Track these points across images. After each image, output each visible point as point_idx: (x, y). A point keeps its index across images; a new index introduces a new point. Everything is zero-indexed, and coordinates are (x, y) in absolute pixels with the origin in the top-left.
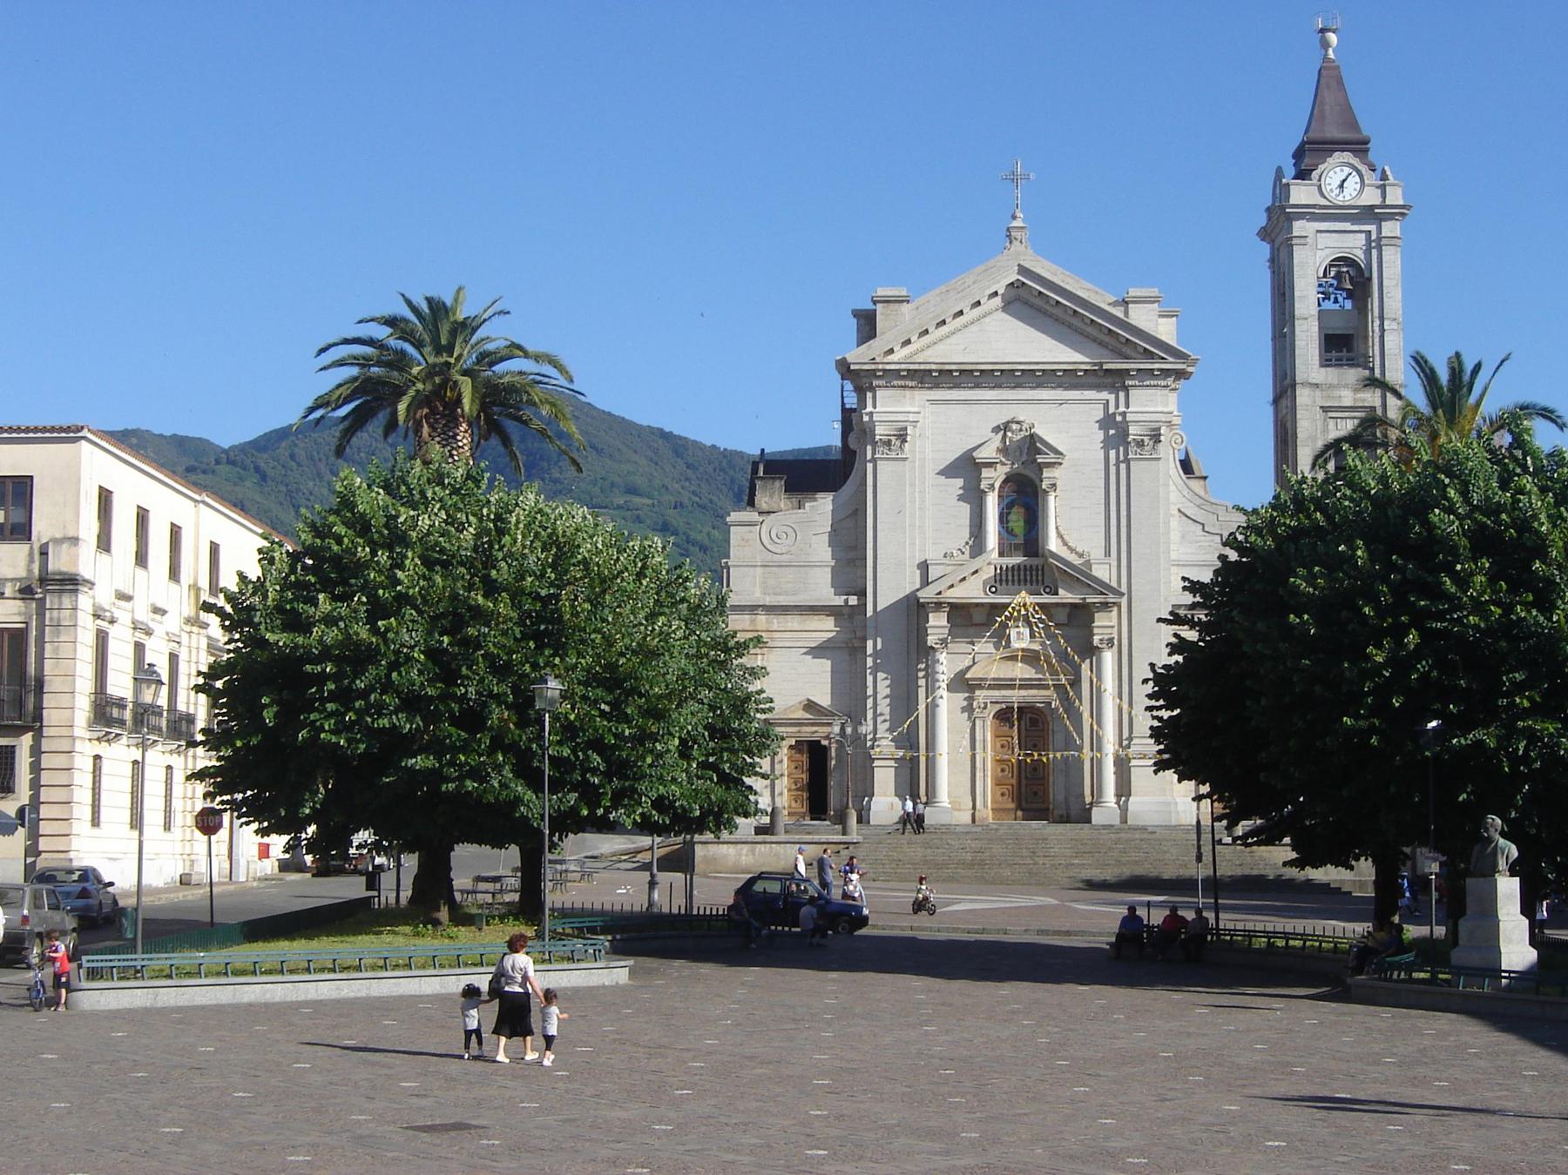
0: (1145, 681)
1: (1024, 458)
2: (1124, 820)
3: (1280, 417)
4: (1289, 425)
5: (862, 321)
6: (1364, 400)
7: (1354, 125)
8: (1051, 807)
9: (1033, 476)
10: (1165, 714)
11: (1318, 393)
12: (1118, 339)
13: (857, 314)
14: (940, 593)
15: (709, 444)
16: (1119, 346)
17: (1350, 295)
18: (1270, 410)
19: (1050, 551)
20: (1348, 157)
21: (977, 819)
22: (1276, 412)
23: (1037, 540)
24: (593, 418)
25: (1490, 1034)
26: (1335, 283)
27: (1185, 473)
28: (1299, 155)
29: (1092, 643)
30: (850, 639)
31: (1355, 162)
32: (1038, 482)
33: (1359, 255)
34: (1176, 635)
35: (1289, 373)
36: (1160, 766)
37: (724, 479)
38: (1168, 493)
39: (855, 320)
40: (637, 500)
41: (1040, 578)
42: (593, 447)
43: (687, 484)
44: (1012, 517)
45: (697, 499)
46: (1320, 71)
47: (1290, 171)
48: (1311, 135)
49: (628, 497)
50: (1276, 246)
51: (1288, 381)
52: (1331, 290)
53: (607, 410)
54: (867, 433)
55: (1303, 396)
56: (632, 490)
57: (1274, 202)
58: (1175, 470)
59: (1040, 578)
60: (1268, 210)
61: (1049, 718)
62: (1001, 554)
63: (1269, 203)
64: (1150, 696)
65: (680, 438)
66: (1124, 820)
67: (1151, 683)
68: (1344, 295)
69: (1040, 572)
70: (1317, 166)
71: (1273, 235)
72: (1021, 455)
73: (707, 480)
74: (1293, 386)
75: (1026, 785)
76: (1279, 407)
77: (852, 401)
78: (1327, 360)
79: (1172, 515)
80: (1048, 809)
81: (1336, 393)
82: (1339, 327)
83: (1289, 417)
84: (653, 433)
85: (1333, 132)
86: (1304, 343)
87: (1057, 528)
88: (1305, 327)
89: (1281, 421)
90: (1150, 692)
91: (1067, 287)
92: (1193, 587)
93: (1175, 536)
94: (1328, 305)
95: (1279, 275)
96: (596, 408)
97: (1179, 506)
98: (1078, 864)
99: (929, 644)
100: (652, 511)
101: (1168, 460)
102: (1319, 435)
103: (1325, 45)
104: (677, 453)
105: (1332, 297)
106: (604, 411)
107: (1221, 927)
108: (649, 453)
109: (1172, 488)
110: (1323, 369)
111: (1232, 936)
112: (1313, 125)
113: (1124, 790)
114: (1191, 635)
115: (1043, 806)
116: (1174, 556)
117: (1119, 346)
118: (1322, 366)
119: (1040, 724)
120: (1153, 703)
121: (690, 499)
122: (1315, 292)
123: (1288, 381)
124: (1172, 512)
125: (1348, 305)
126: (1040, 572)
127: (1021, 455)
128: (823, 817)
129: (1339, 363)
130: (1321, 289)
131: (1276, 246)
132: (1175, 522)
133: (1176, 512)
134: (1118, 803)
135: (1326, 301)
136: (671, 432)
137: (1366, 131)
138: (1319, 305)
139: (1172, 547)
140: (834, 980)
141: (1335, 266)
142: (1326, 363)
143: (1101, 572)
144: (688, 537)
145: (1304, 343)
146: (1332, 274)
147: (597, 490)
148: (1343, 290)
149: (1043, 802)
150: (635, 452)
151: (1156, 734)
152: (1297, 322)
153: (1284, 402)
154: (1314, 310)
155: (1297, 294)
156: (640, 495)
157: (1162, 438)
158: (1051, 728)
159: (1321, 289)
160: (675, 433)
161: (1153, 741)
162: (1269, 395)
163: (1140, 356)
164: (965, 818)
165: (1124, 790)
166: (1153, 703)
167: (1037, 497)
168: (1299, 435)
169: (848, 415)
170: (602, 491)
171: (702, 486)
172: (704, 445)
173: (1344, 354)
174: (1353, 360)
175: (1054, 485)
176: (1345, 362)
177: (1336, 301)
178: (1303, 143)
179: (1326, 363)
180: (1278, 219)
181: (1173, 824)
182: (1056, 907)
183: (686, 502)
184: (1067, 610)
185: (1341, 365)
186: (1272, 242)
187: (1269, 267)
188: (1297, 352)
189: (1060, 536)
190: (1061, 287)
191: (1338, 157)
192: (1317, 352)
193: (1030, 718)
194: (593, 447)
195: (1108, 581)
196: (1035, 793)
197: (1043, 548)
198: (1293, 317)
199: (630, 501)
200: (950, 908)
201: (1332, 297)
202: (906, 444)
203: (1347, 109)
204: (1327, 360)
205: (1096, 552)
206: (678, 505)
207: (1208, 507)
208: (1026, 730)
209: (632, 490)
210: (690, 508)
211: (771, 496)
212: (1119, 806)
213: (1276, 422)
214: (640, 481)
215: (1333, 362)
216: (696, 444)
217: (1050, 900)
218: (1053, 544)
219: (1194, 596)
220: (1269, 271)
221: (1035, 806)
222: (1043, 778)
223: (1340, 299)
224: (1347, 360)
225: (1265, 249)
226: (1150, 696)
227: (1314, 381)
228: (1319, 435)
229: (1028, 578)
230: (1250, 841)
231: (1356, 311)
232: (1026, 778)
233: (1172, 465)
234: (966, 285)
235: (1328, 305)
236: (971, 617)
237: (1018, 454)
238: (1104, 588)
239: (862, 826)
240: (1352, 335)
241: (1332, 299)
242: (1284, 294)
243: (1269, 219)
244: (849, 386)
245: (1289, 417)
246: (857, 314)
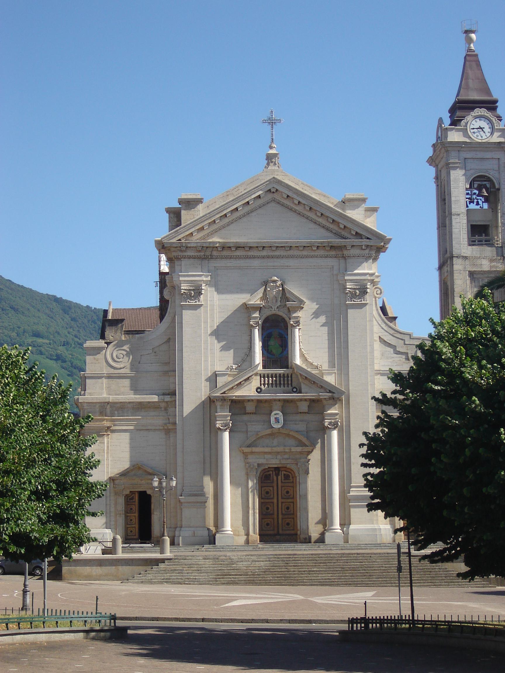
0: (361, 445)
1: (279, 304)
2: (346, 541)
3: (443, 278)
4: (449, 283)
5: (172, 215)
6: (496, 267)
7: (487, 91)
8: (299, 533)
9: (284, 316)
10: (376, 471)
11: (467, 262)
12: (339, 226)
13: (169, 211)
14: (224, 393)
15: (85, 305)
16: (340, 231)
17: (487, 200)
18: (436, 274)
19: (296, 364)
20: (483, 112)
21: (250, 541)
22: (440, 275)
23: (287, 357)
24: (11, 289)
25: (205, 395)
26: (477, 192)
27: (384, 316)
28: (452, 111)
29: (323, 425)
30: (165, 424)
31: (488, 114)
32: (287, 319)
33: (492, 175)
34: (383, 412)
35: (448, 250)
36: (371, 507)
37: (95, 327)
38: (373, 326)
39: (168, 215)
40: (40, 340)
41: (290, 382)
42: (12, 308)
43: (71, 330)
44: (272, 342)
45: (78, 340)
46: (465, 58)
47: (447, 121)
48: (462, 97)
49: (35, 339)
50: (439, 169)
51: (448, 255)
52: (474, 196)
53: (21, 284)
54: (175, 288)
55: (458, 265)
56: (37, 335)
57: (437, 140)
58: (376, 313)
59: (290, 382)
60: (434, 145)
61: (297, 474)
62: (264, 367)
63: (434, 141)
64: (363, 456)
65: (66, 301)
66: (346, 541)
67: (365, 448)
68: (483, 200)
69: (290, 379)
70: (464, 117)
71: (437, 162)
72: (276, 301)
73: (84, 328)
74: (452, 257)
75: (282, 519)
76: (442, 272)
77: (165, 269)
78: (473, 241)
79: (376, 341)
80: (296, 534)
81: (479, 262)
82: (479, 220)
83: (449, 278)
84: (49, 298)
85: (475, 96)
86: (458, 230)
87: (300, 349)
88: (458, 220)
89: (444, 281)
90: (365, 453)
91: (305, 192)
92: (397, 378)
93: (377, 354)
94: (472, 206)
95: (441, 186)
96: (14, 283)
97: (380, 334)
98: (316, 571)
99: (217, 426)
100: (49, 347)
101: (372, 305)
102: (468, 290)
103: (469, 40)
104: (65, 311)
105: (475, 201)
106: (19, 285)
107: (416, 618)
108: (47, 311)
109: (375, 323)
110: (470, 247)
111: (423, 625)
112: (461, 91)
113: (345, 522)
114: (395, 414)
115: (292, 532)
116: (376, 367)
117: (340, 231)
118: (470, 245)
119: (291, 478)
120: (367, 461)
121: (73, 339)
122: (464, 198)
123: (448, 255)
124: (375, 338)
125: (486, 206)
126: (290, 379)
127: (276, 301)
128: (148, 542)
129: (480, 243)
130: (468, 196)
131: (439, 169)
132: (377, 346)
133: (378, 339)
134: (342, 529)
135: (472, 204)
136: (61, 298)
137: (495, 95)
138: (467, 206)
139: (376, 361)
140: (141, 666)
141: (478, 181)
142: (472, 243)
143: (330, 379)
144: (72, 364)
145: (458, 230)
146: (476, 186)
147: (14, 334)
148: (482, 196)
149: (293, 530)
150: (39, 310)
151: (369, 485)
152: (453, 217)
153: (445, 268)
154: (464, 209)
155: (453, 199)
156: (42, 338)
157: (368, 290)
158: (298, 480)
159: (468, 196)
160: (64, 298)
161: (367, 489)
162: (435, 263)
163: (352, 237)
164: (242, 539)
165: (345, 522)
166: (367, 461)
167: (287, 329)
168: (456, 290)
169: (163, 277)
170: (17, 335)
171: (81, 331)
172: (82, 306)
173: (483, 237)
174: (489, 241)
175: (299, 322)
176: (484, 243)
177: (478, 204)
178: (455, 103)
179: (472, 243)
180: (440, 151)
181: (378, 542)
182: (301, 602)
183: (71, 341)
184: (307, 403)
185: (482, 244)
186: (436, 166)
187: (435, 182)
188: (453, 236)
189: (302, 355)
190: (302, 192)
191: (478, 112)
192: (466, 236)
193: (284, 475)
194: (12, 308)
195: (334, 385)
196: (288, 524)
197: (292, 363)
198: (451, 214)
199: (35, 341)
200: (227, 605)
201: (475, 201)
202: (202, 296)
203: (483, 81)
204: (473, 241)
205: (325, 366)
206: (65, 344)
207: (398, 335)
208: (282, 482)
209: (37, 335)
210: (73, 346)
211: (116, 332)
212: (343, 531)
213: (440, 281)
214: (41, 329)
215: (477, 243)
216: (78, 306)
217: (298, 596)
218: (298, 361)
219: (396, 386)
220: (434, 185)
221: (288, 532)
222: (293, 514)
223: (480, 202)
224: (486, 241)
225: (432, 171)
226: (363, 456)
227: (465, 255)
228: (468, 290)
229: (282, 382)
230: (436, 558)
231: (491, 210)
232: (282, 514)
233: (375, 313)
234: (240, 191)
235: (472, 206)
236: (245, 408)
237: (274, 301)
238: (330, 390)
239: (175, 548)
240: (489, 225)
241: (475, 203)
242: (445, 200)
243: (434, 151)
244: (163, 257)
245: (449, 278)
246: (169, 211)
